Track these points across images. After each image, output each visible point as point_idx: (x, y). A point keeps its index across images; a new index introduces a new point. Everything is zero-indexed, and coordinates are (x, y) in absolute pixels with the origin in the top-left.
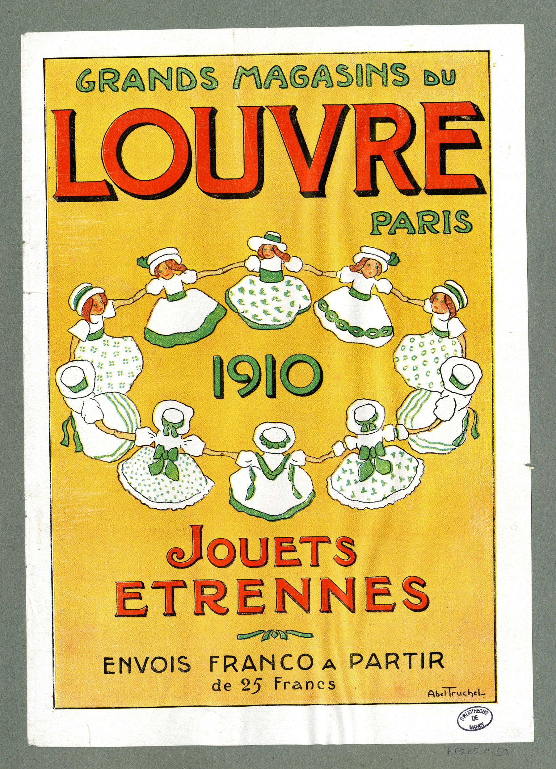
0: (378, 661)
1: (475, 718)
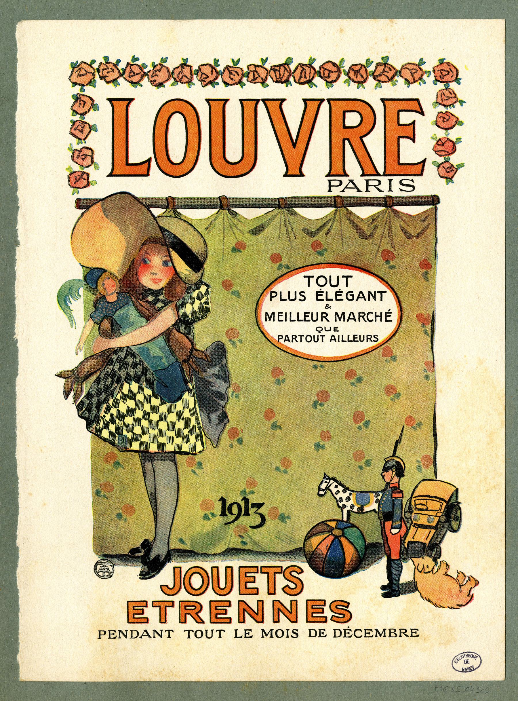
0: (354, 317)
1: (467, 662)
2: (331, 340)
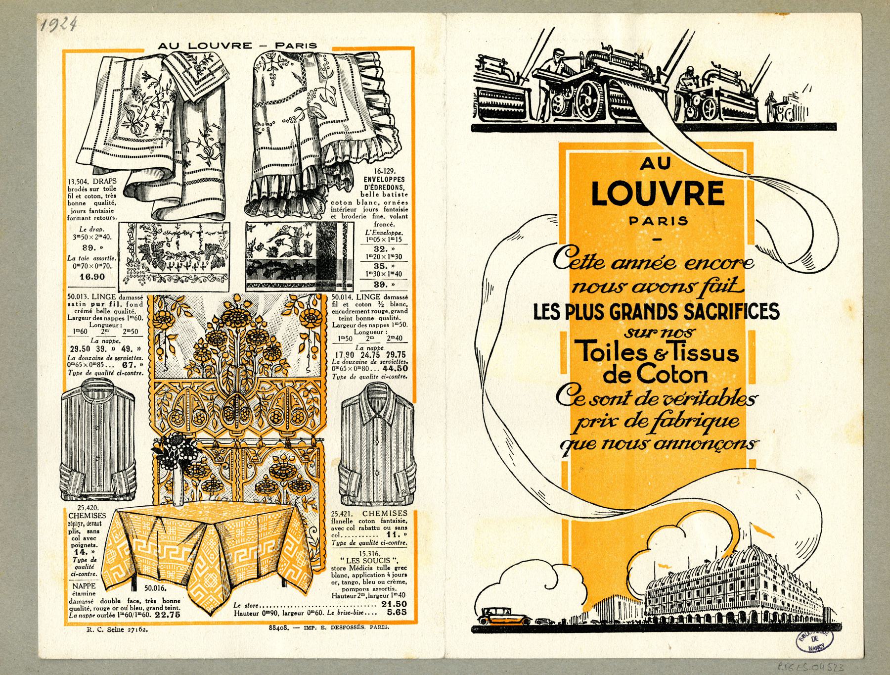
1: (815, 639)
2: (631, 223)
